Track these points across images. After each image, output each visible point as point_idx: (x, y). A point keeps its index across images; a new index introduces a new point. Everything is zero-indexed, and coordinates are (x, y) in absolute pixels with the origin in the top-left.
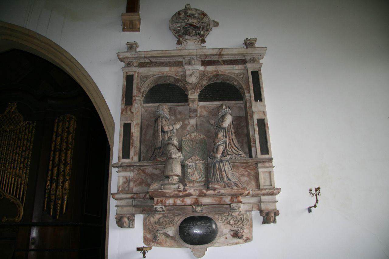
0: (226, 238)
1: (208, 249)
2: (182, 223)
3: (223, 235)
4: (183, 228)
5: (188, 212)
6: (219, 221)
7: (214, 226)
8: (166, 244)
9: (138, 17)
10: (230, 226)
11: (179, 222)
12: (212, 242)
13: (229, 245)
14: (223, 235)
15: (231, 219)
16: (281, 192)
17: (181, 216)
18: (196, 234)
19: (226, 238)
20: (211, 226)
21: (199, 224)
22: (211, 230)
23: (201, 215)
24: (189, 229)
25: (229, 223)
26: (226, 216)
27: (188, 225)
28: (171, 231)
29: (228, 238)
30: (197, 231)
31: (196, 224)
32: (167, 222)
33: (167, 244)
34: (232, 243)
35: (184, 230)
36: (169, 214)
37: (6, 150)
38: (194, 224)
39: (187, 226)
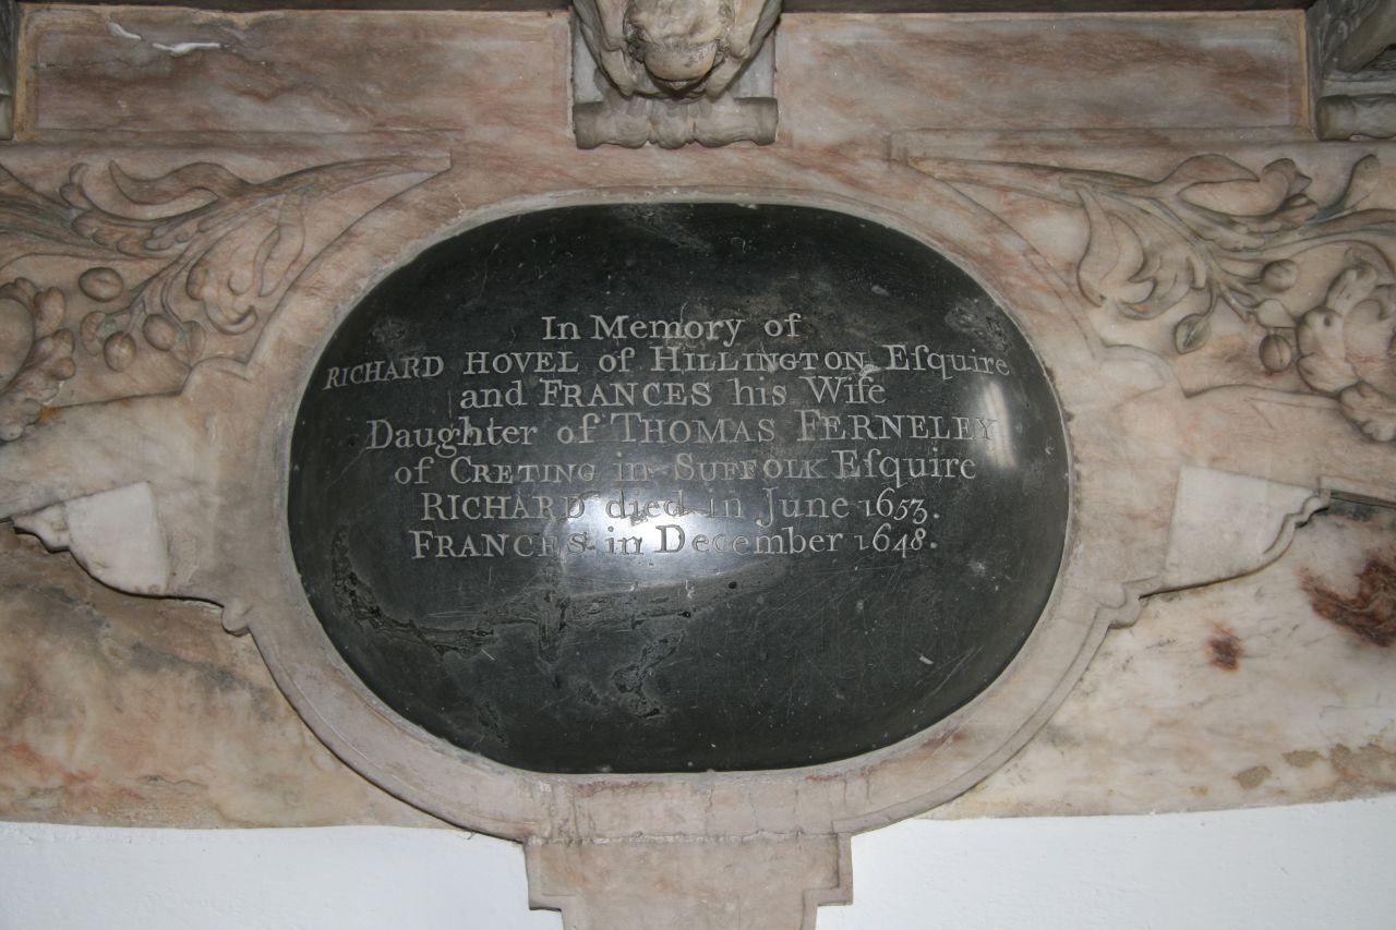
0: (1226, 653)
1: (866, 851)
2: (354, 340)
3: (1169, 592)
4: (383, 435)
5: (487, 134)
6: (1102, 322)
7: (992, 425)
8: (28, 754)
9: (1162, 556)
10: (1313, 415)
11: (306, 321)
12: (950, 721)
13: (1283, 796)
14: (1169, 592)
15: (1335, 282)
16: (591, 79)
17: (352, 208)
18: (614, 566)
19: (1226, 653)
20: (948, 401)
21: (698, 344)
22: (950, 486)
23: (748, 198)
24: (487, 455)
25: (1285, 355)
26: (1230, 221)
27: (477, 361)
28: (139, 495)
29: (1250, 645)
30: (644, 533)
31: (643, 347)
32: (54, 308)
33: (56, 748)
34: (1340, 751)
35: (396, 457)
36: (97, 164)
37: (948, 21)
38: (588, 351)
39: (459, 381)
